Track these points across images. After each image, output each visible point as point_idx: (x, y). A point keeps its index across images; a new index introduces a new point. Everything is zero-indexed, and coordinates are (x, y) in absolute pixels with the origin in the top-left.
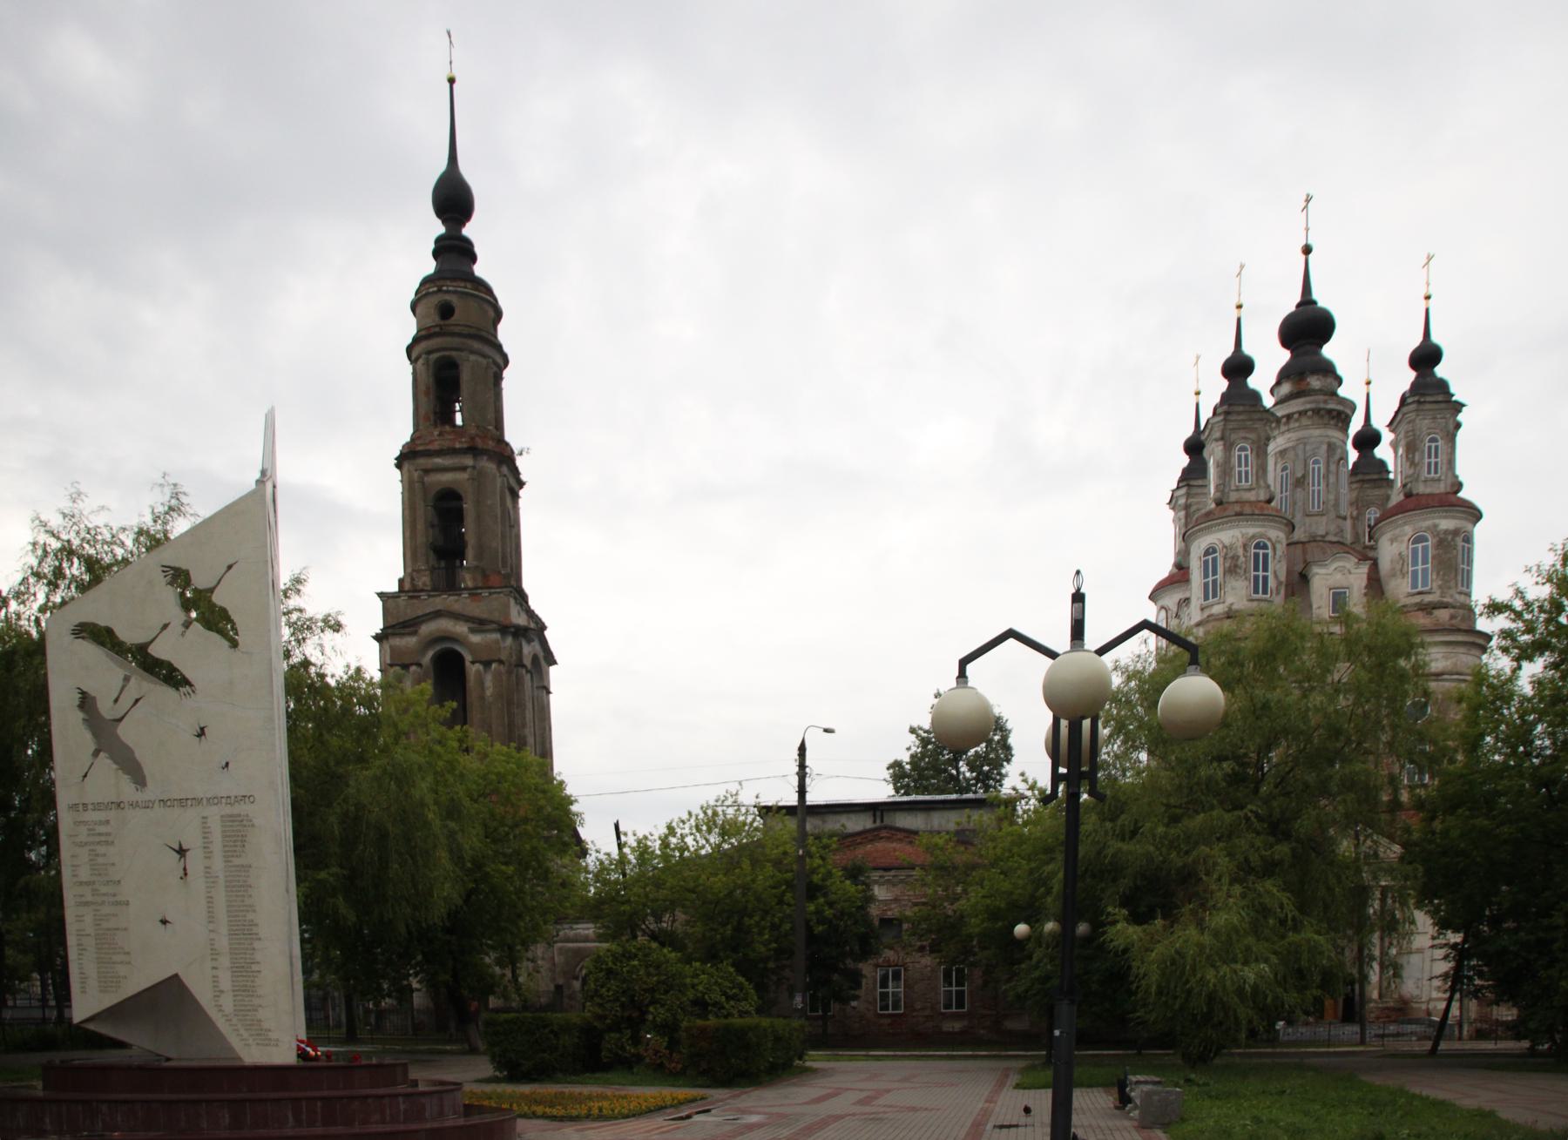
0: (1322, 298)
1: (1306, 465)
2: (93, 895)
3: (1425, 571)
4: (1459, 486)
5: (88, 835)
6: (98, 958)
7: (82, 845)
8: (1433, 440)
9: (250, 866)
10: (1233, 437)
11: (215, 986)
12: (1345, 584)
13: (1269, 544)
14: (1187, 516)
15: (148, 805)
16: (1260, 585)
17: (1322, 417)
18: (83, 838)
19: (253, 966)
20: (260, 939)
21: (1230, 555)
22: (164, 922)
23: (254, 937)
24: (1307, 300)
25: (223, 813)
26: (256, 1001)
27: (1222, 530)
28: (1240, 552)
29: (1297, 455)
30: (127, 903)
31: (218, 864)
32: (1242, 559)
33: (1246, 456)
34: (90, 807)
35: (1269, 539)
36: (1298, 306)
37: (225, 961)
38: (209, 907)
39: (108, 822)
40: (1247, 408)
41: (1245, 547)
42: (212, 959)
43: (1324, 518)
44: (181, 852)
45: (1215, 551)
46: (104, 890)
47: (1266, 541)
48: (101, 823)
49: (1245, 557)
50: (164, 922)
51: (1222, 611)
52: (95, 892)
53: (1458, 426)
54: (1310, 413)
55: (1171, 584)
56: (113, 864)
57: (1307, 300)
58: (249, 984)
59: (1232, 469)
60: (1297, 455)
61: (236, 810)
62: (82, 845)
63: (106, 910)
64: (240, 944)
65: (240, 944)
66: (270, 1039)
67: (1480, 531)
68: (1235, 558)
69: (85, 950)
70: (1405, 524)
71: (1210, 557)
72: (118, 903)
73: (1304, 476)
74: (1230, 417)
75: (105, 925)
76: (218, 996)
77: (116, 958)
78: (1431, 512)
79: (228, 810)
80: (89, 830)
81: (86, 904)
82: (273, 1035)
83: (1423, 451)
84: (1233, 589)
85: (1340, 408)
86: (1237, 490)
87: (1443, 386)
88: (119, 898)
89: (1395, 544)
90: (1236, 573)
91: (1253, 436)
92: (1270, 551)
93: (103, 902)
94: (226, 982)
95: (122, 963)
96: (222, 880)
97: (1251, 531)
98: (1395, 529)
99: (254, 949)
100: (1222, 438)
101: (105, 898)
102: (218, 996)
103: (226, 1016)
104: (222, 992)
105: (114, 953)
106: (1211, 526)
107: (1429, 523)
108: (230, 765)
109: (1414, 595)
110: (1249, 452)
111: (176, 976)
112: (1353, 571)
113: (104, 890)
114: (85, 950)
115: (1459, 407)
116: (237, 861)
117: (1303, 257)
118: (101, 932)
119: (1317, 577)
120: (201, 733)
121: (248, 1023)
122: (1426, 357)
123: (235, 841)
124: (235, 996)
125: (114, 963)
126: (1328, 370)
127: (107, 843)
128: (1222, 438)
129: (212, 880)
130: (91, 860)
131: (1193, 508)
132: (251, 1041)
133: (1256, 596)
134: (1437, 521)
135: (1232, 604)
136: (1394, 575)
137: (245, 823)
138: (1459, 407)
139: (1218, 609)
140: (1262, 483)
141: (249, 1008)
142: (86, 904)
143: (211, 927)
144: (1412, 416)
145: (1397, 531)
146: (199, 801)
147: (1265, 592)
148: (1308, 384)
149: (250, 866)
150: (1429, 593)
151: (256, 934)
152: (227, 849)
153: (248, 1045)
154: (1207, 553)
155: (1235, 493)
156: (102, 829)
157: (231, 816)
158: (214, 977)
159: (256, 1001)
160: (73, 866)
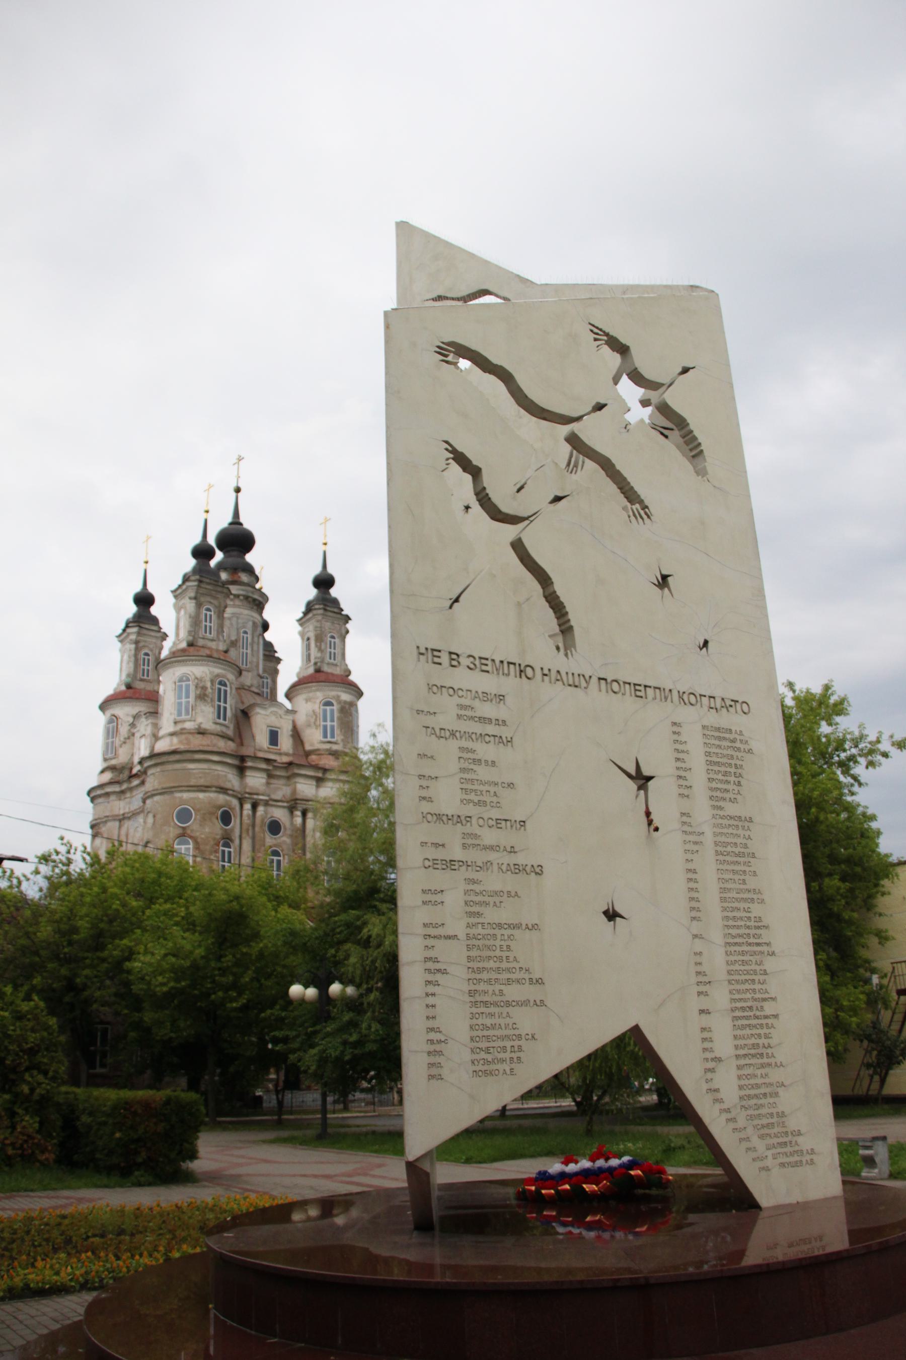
0: (248, 523)
1: (238, 633)
2: (464, 846)
3: (332, 727)
4: (349, 673)
5: (459, 717)
6: (471, 993)
7: (443, 734)
8: (333, 637)
9: (751, 820)
10: (202, 599)
11: (705, 1050)
12: (278, 725)
13: (228, 683)
14: (137, 650)
15: (578, 682)
16: (220, 713)
17: (249, 602)
18: (447, 719)
19: (766, 1005)
20: (773, 954)
21: (201, 685)
22: (611, 915)
23: (764, 948)
24: (236, 521)
25: (706, 722)
26: (775, 1075)
27: (194, 665)
28: (209, 684)
29: (231, 624)
30: (538, 871)
31: (702, 811)
32: (209, 690)
33: (211, 616)
34: (465, 661)
35: (228, 680)
36: (231, 524)
37: (720, 998)
38: (691, 889)
39: (501, 698)
40: (212, 582)
41: (212, 682)
42: (700, 993)
43: (250, 674)
44: (642, 780)
45: (188, 680)
46: (489, 837)
47: (226, 681)
48: (486, 697)
49: (212, 689)
50: (611, 915)
51: (193, 727)
52: (470, 842)
53: (347, 632)
54: (241, 598)
55: (116, 699)
56: (511, 785)
57: (236, 521)
58: (761, 1042)
59: (201, 622)
60: (231, 624)
61: (726, 719)
62: (443, 734)
63: (493, 881)
64: (744, 963)
65: (744, 963)
66: (800, 1152)
67: (361, 704)
68: (204, 688)
69: (444, 972)
70: (317, 690)
71: (184, 684)
72: (518, 869)
73: (236, 640)
74: (203, 585)
75: (491, 915)
76: (712, 1070)
77: (513, 992)
78: (336, 686)
79: (712, 719)
80: (461, 707)
81: (450, 864)
82: (805, 1143)
83: (326, 644)
84: (202, 711)
85: (260, 599)
86: (203, 638)
87: (335, 602)
88: (521, 859)
89: (309, 703)
90: (205, 700)
91: (216, 602)
92: (228, 689)
93: (488, 864)
94: (724, 1045)
95: (526, 1003)
96: (709, 839)
97: (217, 671)
98: (309, 692)
99: (765, 973)
100: (195, 598)
101: (492, 856)
102: (712, 1070)
103: (728, 1111)
104: (718, 1060)
105: (509, 982)
106: (186, 661)
107: (333, 693)
108: (710, 644)
109: (324, 743)
110: (212, 613)
111: (636, 1030)
112: (283, 717)
113: (489, 837)
114: (444, 972)
115: (347, 618)
116: (731, 809)
117: (234, 494)
118: (479, 930)
119: (259, 716)
120: (664, 581)
121: (765, 1121)
122: (324, 582)
123: (726, 774)
124: (739, 1067)
125: (508, 1004)
126: (249, 569)
127: (500, 740)
128: (195, 598)
129: (693, 838)
130: (463, 770)
131: (141, 644)
132: (769, 1162)
133: (218, 721)
134: (340, 693)
135: (201, 723)
136: (309, 725)
137: (738, 745)
138: (347, 618)
139: (189, 725)
140: (221, 638)
141: (762, 1090)
142: (450, 864)
143: (696, 928)
144: (320, 618)
145: (311, 695)
146: (664, 693)
147: (225, 719)
148: (239, 577)
149: (751, 820)
150: (335, 743)
151: (768, 944)
152: (714, 785)
153: (767, 1169)
154: (181, 680)
155: (201, 640)
156: (487, 710)
157: (718, 729)
158: (703, 1029)
159: (775, 1075)
160: (421, 776)
